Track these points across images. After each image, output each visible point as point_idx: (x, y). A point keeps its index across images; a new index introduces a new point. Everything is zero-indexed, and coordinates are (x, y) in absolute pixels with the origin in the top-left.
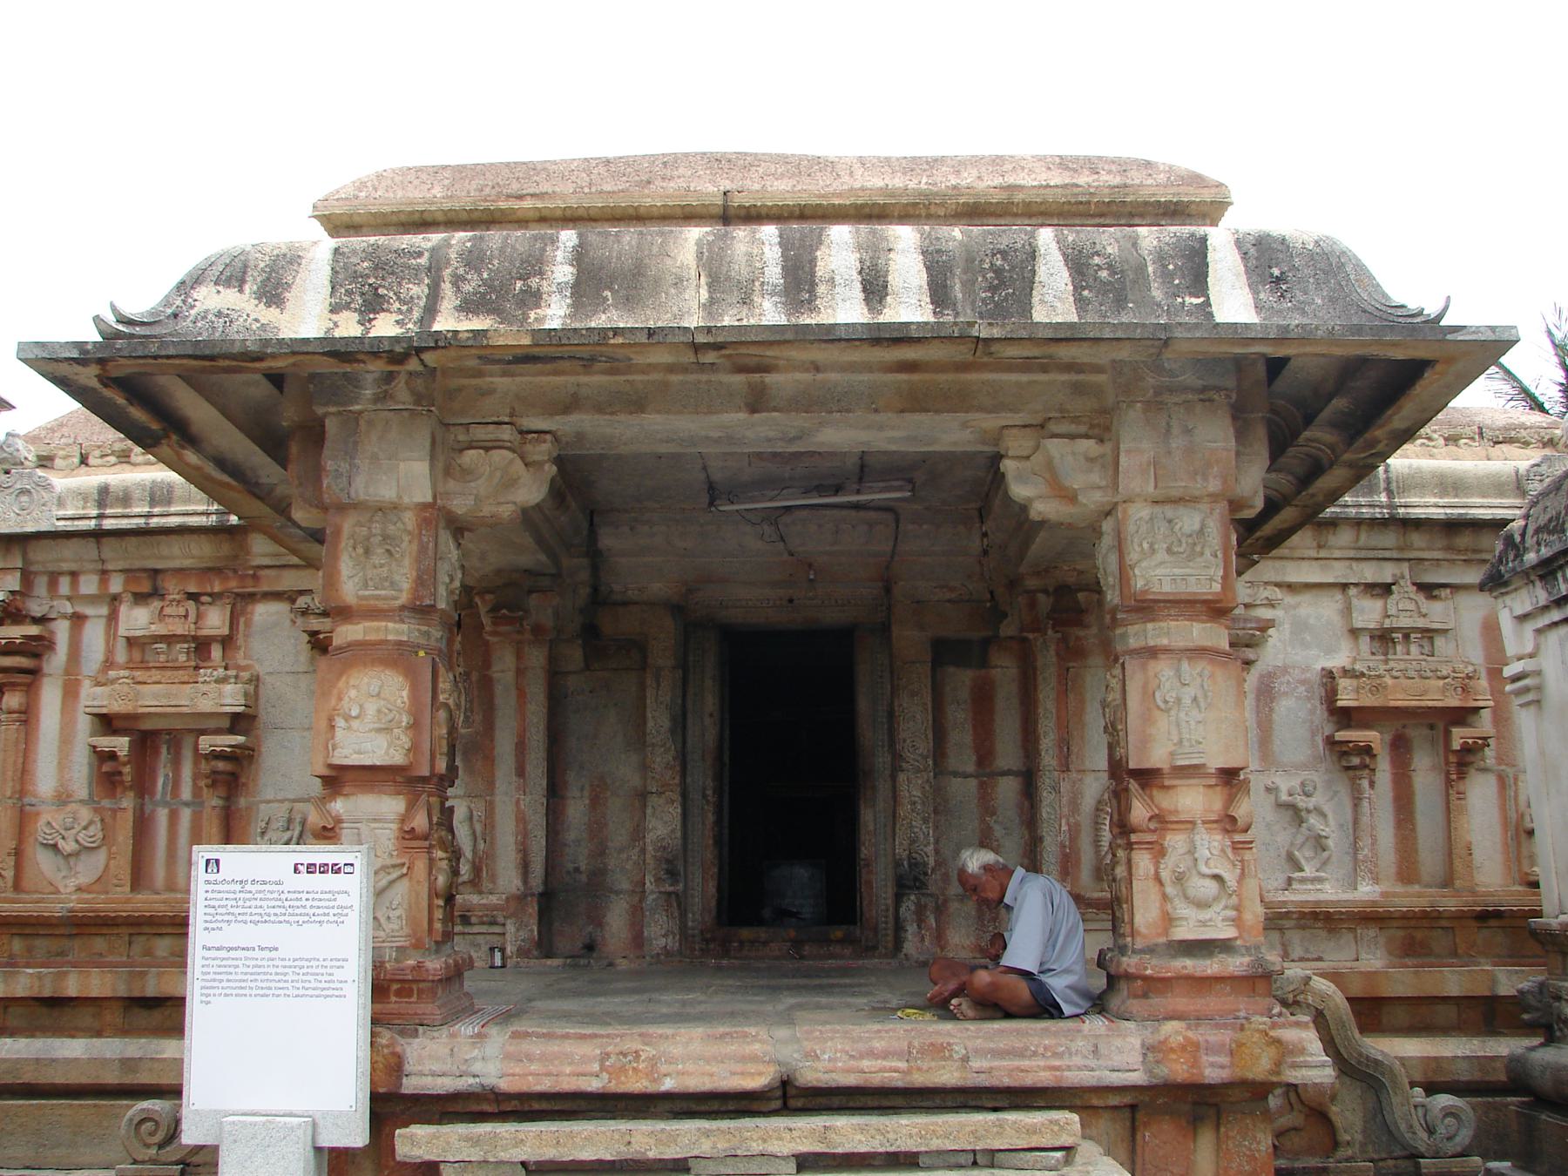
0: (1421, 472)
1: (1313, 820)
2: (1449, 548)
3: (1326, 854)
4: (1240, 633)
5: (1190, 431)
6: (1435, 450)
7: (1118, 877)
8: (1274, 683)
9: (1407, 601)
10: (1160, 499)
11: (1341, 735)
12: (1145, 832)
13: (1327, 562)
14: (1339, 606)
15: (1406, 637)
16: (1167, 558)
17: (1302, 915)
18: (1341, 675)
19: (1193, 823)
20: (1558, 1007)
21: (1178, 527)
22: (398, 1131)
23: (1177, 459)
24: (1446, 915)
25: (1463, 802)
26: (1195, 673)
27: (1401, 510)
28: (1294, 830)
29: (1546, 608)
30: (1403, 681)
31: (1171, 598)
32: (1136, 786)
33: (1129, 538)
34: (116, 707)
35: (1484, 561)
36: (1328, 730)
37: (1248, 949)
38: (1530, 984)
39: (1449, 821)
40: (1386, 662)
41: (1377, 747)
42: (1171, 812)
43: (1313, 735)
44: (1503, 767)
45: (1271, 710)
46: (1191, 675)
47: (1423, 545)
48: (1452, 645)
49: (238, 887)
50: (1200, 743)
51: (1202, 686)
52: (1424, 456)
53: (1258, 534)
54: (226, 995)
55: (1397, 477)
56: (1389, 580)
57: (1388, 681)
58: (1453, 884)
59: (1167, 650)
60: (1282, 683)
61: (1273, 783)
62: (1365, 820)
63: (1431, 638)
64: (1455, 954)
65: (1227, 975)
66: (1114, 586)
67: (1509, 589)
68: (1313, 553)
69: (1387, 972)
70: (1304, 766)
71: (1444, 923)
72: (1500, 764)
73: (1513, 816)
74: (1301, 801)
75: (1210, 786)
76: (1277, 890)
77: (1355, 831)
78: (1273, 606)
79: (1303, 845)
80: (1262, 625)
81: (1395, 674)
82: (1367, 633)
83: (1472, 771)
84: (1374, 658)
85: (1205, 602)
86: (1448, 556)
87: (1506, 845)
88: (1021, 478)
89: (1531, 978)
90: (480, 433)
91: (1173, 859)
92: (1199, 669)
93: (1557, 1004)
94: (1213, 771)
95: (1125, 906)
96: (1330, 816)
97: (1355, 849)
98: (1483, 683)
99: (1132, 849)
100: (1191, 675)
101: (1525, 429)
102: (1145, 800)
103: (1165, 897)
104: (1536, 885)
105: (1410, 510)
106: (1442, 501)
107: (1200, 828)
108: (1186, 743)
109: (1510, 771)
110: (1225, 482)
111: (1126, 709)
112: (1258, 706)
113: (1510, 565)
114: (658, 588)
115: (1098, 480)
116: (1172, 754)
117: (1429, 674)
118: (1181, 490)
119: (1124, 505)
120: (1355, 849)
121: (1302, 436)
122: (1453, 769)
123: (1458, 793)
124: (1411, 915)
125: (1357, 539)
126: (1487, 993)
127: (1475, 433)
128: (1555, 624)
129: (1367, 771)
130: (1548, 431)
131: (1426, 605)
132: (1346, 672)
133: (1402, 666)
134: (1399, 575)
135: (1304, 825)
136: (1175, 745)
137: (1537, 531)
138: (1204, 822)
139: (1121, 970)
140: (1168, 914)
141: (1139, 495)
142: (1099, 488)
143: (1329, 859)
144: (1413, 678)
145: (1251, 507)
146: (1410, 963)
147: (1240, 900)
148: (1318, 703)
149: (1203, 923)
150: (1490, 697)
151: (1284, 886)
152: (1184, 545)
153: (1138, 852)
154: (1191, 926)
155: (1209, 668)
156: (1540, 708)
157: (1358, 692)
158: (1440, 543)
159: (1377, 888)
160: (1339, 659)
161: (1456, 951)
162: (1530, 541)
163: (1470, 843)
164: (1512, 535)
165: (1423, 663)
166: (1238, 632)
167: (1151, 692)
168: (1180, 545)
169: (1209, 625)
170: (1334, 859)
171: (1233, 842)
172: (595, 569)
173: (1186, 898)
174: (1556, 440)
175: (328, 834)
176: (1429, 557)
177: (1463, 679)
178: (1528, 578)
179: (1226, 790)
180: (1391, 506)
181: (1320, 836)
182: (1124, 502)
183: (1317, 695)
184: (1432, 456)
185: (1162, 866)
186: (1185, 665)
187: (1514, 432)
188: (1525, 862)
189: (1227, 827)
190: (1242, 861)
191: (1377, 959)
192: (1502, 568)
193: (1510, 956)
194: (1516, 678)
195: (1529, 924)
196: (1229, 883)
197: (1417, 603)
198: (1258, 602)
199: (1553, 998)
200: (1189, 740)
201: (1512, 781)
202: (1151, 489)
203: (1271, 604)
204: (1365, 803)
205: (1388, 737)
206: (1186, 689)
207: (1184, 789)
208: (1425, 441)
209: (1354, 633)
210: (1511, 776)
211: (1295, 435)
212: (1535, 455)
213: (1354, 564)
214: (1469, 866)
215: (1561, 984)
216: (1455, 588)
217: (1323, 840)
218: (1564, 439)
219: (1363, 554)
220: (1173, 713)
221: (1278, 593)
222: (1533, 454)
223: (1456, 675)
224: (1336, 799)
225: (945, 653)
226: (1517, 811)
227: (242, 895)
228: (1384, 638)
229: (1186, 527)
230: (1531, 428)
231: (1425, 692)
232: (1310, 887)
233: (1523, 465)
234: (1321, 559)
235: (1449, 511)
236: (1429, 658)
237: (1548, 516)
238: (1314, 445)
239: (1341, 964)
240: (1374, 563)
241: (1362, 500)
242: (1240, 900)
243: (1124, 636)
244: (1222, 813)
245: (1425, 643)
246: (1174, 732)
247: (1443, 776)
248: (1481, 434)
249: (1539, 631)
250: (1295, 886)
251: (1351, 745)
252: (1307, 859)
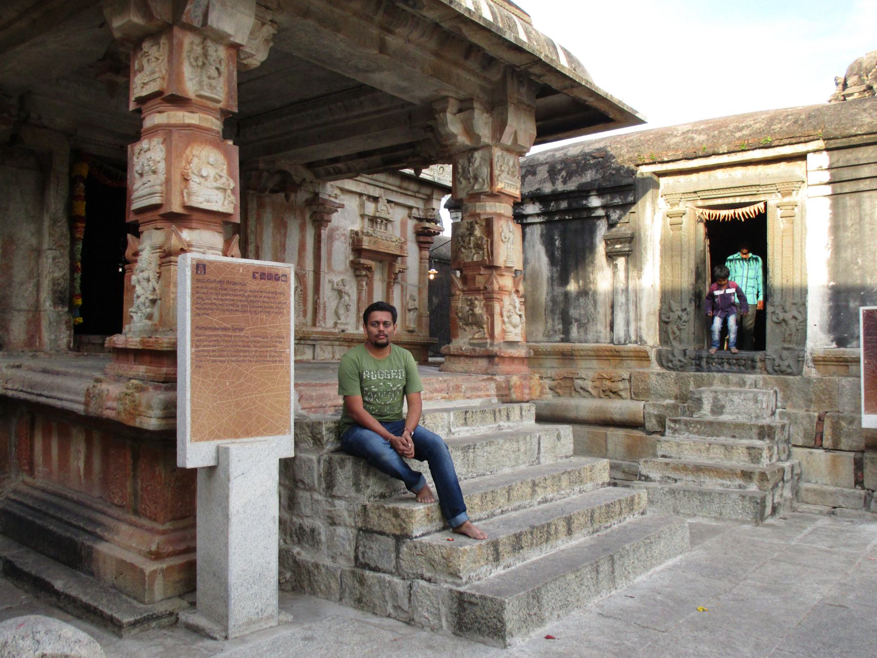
54: (213, 361)
56: (377, 196)
70: (341, 273)
109: (405, 284)
160: (357, 227)
183: (348, 242)
188: (407, 323)
209: (363, 216)
213: (367, 186)
227: (221, 292)
228: (373, 220)
231: (389, 247)
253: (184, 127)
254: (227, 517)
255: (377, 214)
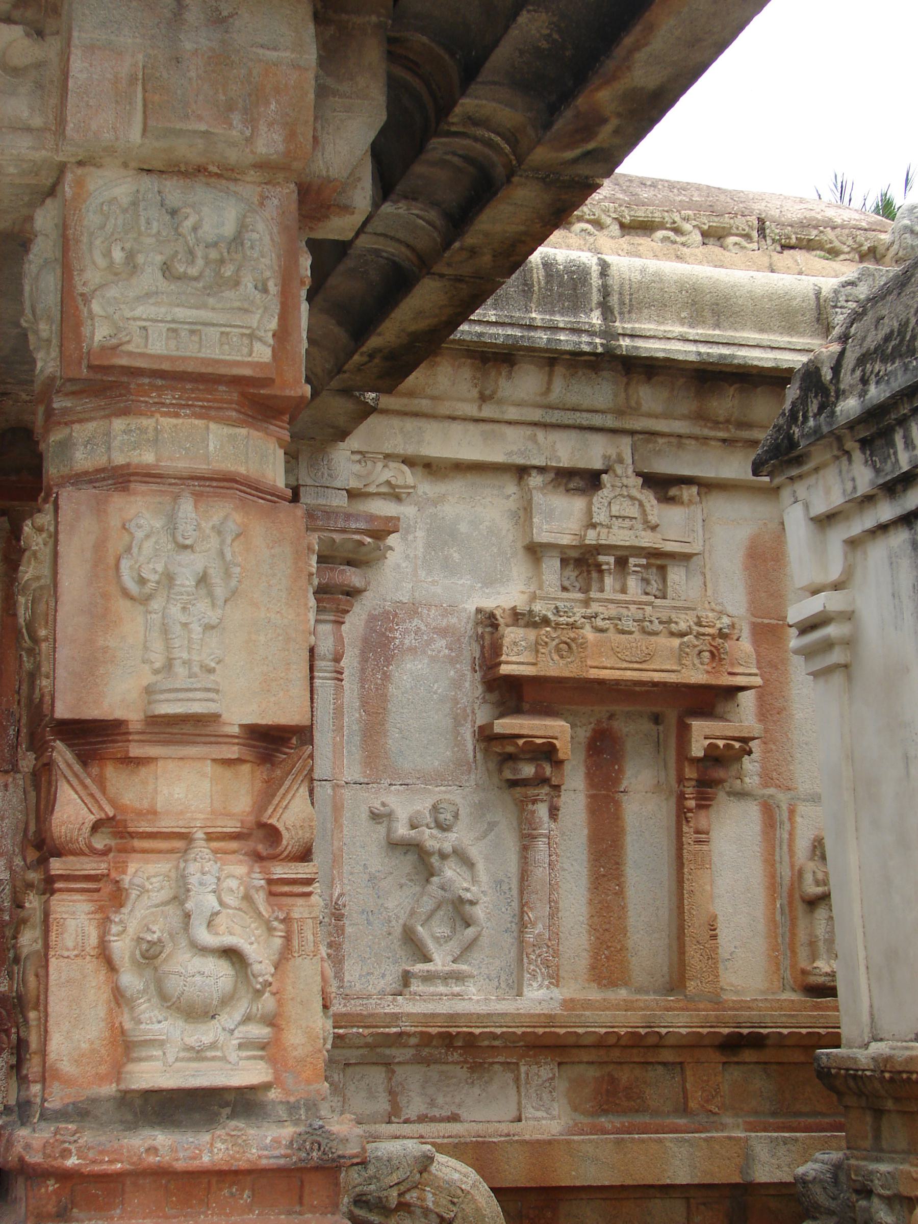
0: (661, 281)
1: (451, 872)
2: (700, 417)
3: (471, 932)
4: (337, 537)
5: (223, 20)
6: (685, 249)
7: (25, 951)
8: (391, 630)
9: (627, 502)
10: (158, 165)
11: (506, 725)
12: (83, 854)
13: (496, 427)
14: (512, 504)
15: (622, 563)
16: (163, 284)
17: (426, 1039)
18: (509, 620)
19: (186, 837)
20: (867, 1210)
21: (188, 223)
23: (193, 74)
24: (670, 1041)
25: (705, 848)
26: (207, 526)
27: (625, 342)
28: (418, 889)
29: (868, 500)
30: (612, 635)
31: (166, 366)
32: (69, 756)
33: (85, 239)
35: (754, 443)
36: (482, 718)
37: (292, 1108)
38: (816, 1166)
39: (680, 881)
40: (587, 603)
41: (564, 748)
42: (140, 814)
43: (457, 723)
44: (771, 791)
45: (386, 677)
46: (198, 527)
47: (657, 407)
48: (697, 581)
50: (211, 671)
51: (222, 554)
52: (667, 257)
53: (374, 342)
55: (622, 285)
56: (598, 465)
57: (588, 633)
58: (685, 987)
59: (150, 476)
60: (406, 631)
61: (383, 804)
62: (540, 873)
63: (662, 569)
64: (684, 1110)
65: (243, 1165)
66: (49, 341)
67: (806, 468)
68: (471, 410)
69: (568, 1142)
70: (438, 778)
71: (667, 1056)
72: (766, 786)
73: (785, 872)
74: (431, 839)
75: (228, 763)
76: (383, 993)
77: (521, 892)
78: (398, 498)
79: (430, 916)
80: (376, 525)
81: (599, 623)
82: (556, 553)
83: (721, 796)
84: (565, 595)
85: (236, 381)
86: (697, 430)
87: (772, 922)
89: (818, 1155)
91: (140, 913)
92: (216, 520)
93: (863, 1203)
94: (236, 730)
95: (32, 1015)
96: (480, 866)
97: (522, 925)
98: (745, 645)
99: (53, 892)
100: (198, 527)
101: (834, 228)
102: (85, 787)
103: (119, 997)
104: (828, 991)
105: (640, 343)
106: (692, 333)
107: (201, 848)
108: (180, 670)
109: (783, 798)
110: (291, 136)
111: (56, 592)
112: (363, 671)
113: (811, 423)
115: (26, 114)
116: (149, 691)
117: (657, 627)
118: (200, 143)
119: (79, 171)
120: (522, 925)
121: (457, 110)
122: (689, 791)
123: (697, 832)
124: (612, 1040)
125: (548, 390)
126: (736, 1179)
127: (751, 227)
128: (883, 528)
129: (546, 789)
130: (871, 234)
131: (655, 510)
132: (516, 617)
133: (613, 611)
134: (614, 457)
135: (435, 879)
136: (156, 672)
137: (862, 361)
138: (210, 837)
139: (12, 1158)
140: (123, 1032)
141: (110, 151)
142: (29, 129)
143: (475, 941)
144: (631, 633)
145: (346, 209)
146: (609, 1126)
147: (280, 1003)
148: (466, 669)
149: (198, 1054)
150: (755, 671)
151: (396, 986)
152: (200, 262)
153: (65, 896)
154: (171, 1059)
155: (237, 517)
156: (849, 678)
157: (537, 651)
158: (687, 405)
159: (557, 994)
161: (686, 1103)
162: (848, 379)
163: (715, 917)
164: (818, 370)
165: (648, 609)
166: (335, 536)
167: (111, 561)
168: (192, 262)
169: (243, 431)
170: (484, 941)
171: (270, 882)
173: (163, 997)
174: (881, 250)
176: (666, 430)
177: (713, 637)
178: (841, 447)
179: (262, 773)
180: (608, 334)
181: (461, 900)
182: (80, 163)
183: (467, 656)
184: (679, 258)
185: (115, 929)
186: (187, 507)
187: (815, 232)
188: (803, 954)
189: (260, 848)
190: (286, 921)
191: (553, 1118)
192: (796, 431)
193: (774, 1114)
194: (808, 627)
195: (817, 1059)
196: (256, 968)
197: (641, 505)
198: (372, 489)
199: (857, 1192)
200: (187, 663)
201: (785, 815)
202: (135, 134)
203: (395, 494)
204: (541, 845)
205: (584, 734)
206: (186, 557)
207: (171, 765)
208: (671, 234)
210: (784, 807)
211: (445, 109)
212: (848, 270)
213: (540, 434)
214: (712, 957)
215: (873, 1166)
216: (707, 486)
217: (467, 907)
218: (896, 247)
219: (556, 417)
220: (155, 605)
221: (406, 476)
222: (844, 269)
223: (702, 630)
224: (491, 836)
226: (792, 866)
229: (206, 227)
230: (843, 227)
231: (649, 657)
232: (442, 989)
233: (828, 284)
234: (483, 420)
235: (703, 349)
236: (658, 602)
237: (881, 334)
238: (480, 132)
239: (491, 1128)
240: (574, 434)
241: (561, 320)
242: (280, 1003)
243: (66, 445)
244: (251, 819)
245: (653, 575)
246: (157, 645)
247: (673, 800)
248: (762, 230)
249: (853, 543)
250: (416, 986)
251: (521, 742)
252: (437, 940)
253: (257, 489)
254: (387, 107)
255: (591, 537)
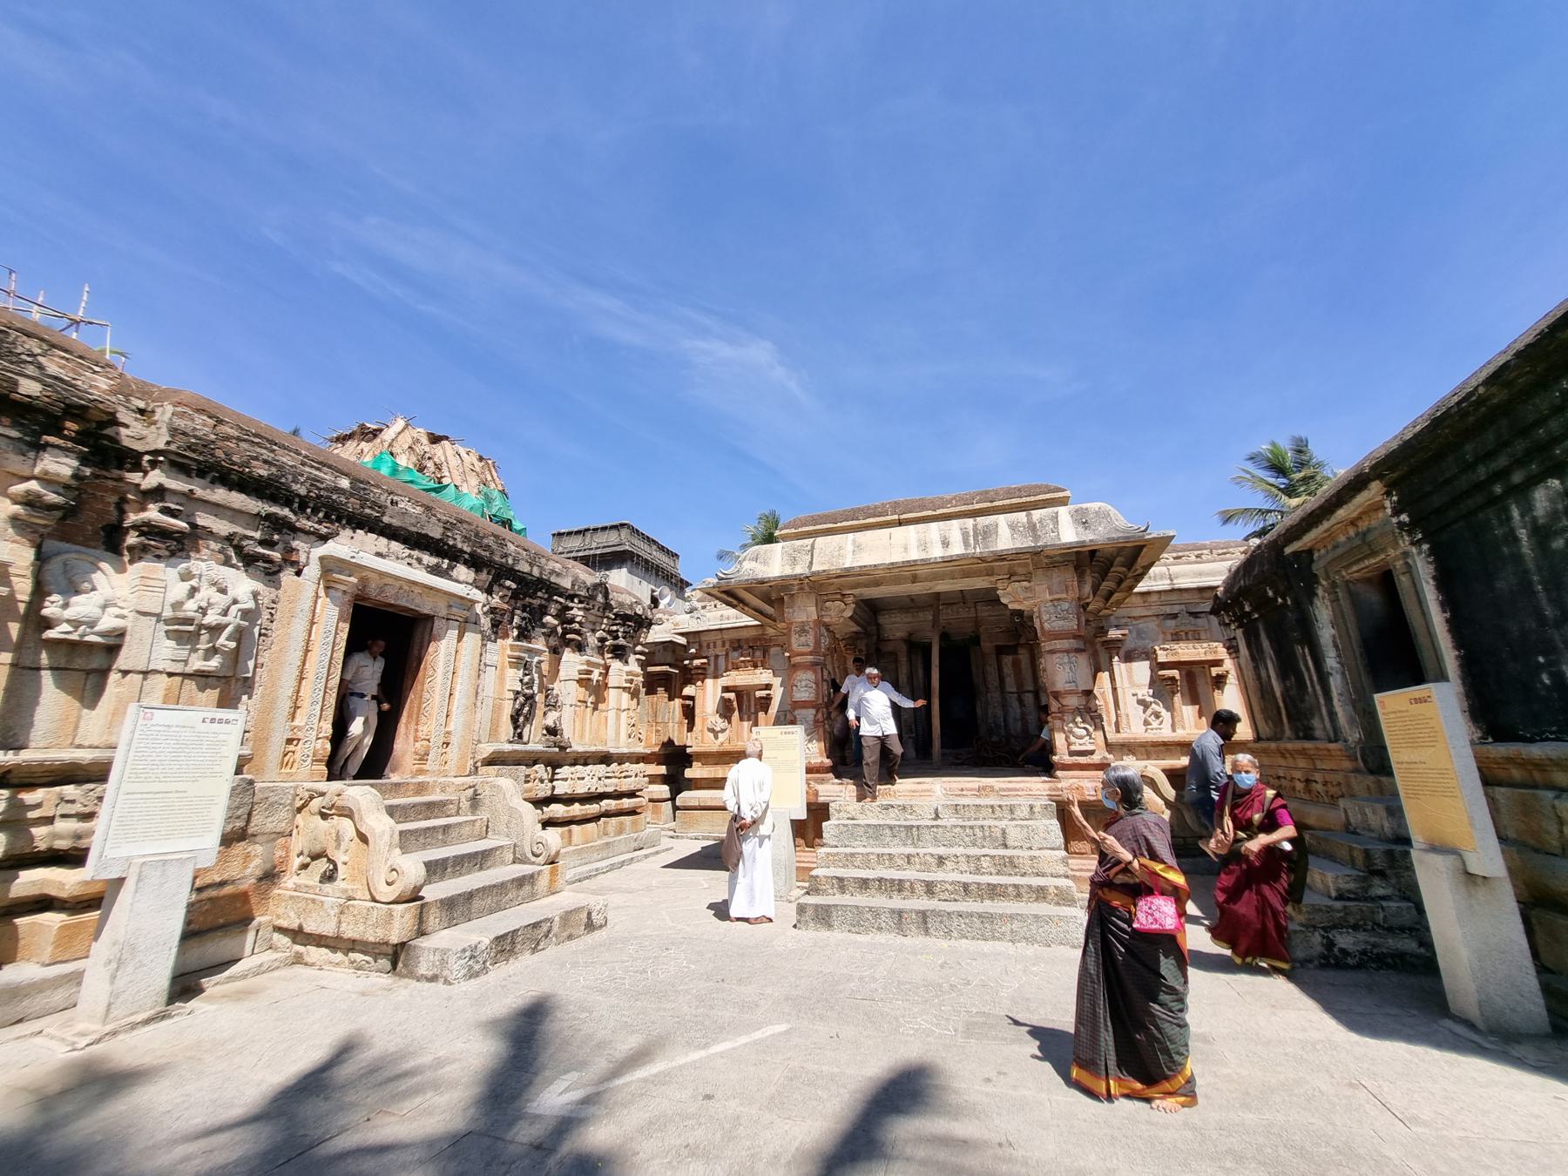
22: (824, 824)
34: (730, 684)
49: (166, 729)
88: (1004, 595)
90: (830, 597)
114: (899, 634)
172: (878, 630)
175: (793, 722)
225: (1000, 651)
